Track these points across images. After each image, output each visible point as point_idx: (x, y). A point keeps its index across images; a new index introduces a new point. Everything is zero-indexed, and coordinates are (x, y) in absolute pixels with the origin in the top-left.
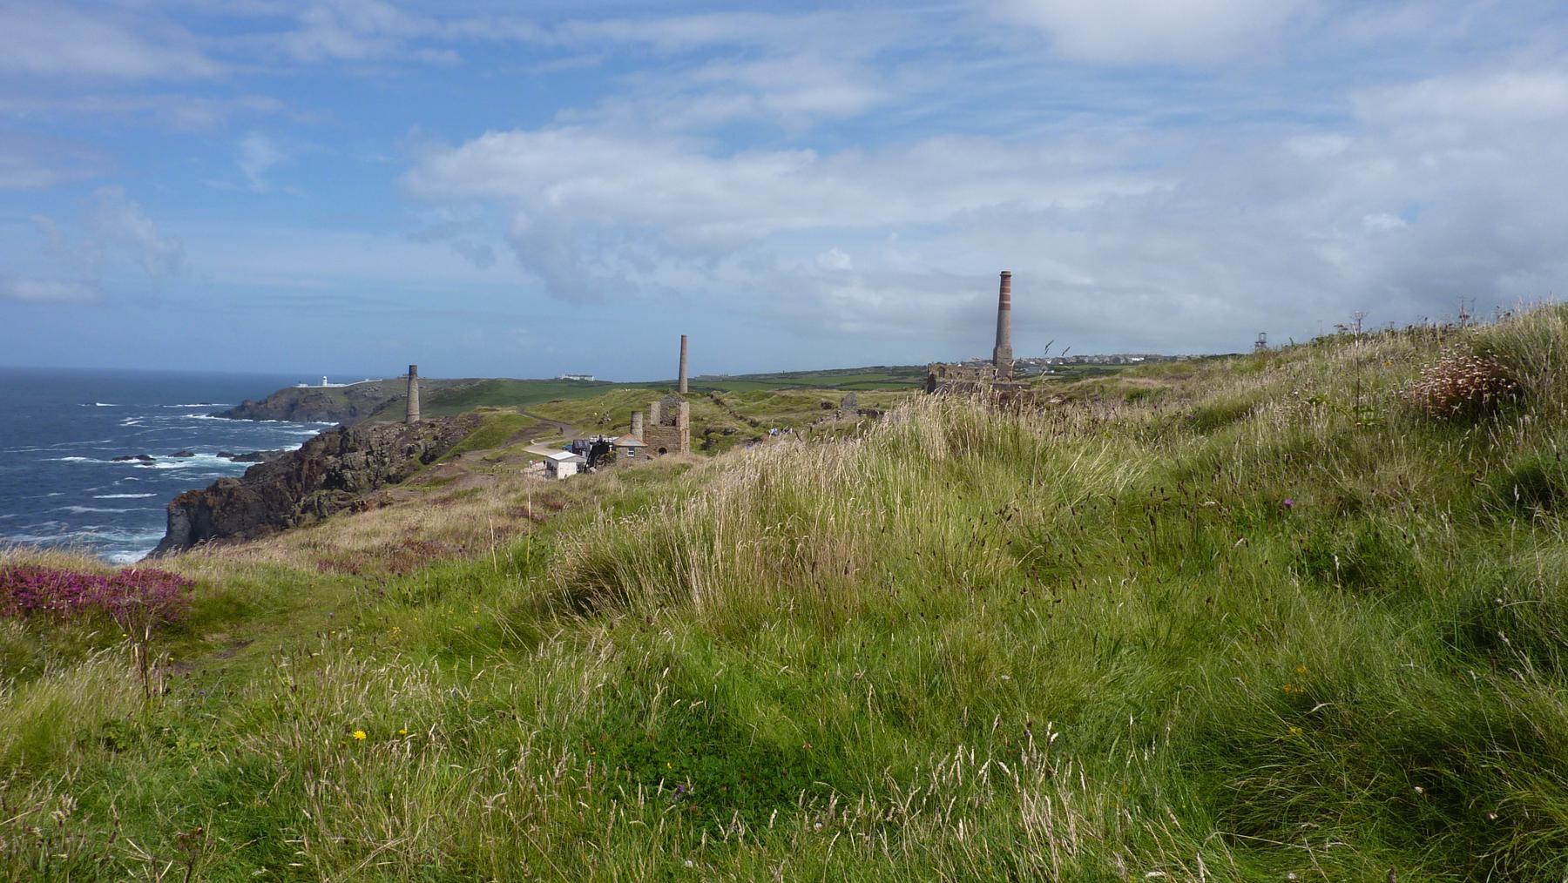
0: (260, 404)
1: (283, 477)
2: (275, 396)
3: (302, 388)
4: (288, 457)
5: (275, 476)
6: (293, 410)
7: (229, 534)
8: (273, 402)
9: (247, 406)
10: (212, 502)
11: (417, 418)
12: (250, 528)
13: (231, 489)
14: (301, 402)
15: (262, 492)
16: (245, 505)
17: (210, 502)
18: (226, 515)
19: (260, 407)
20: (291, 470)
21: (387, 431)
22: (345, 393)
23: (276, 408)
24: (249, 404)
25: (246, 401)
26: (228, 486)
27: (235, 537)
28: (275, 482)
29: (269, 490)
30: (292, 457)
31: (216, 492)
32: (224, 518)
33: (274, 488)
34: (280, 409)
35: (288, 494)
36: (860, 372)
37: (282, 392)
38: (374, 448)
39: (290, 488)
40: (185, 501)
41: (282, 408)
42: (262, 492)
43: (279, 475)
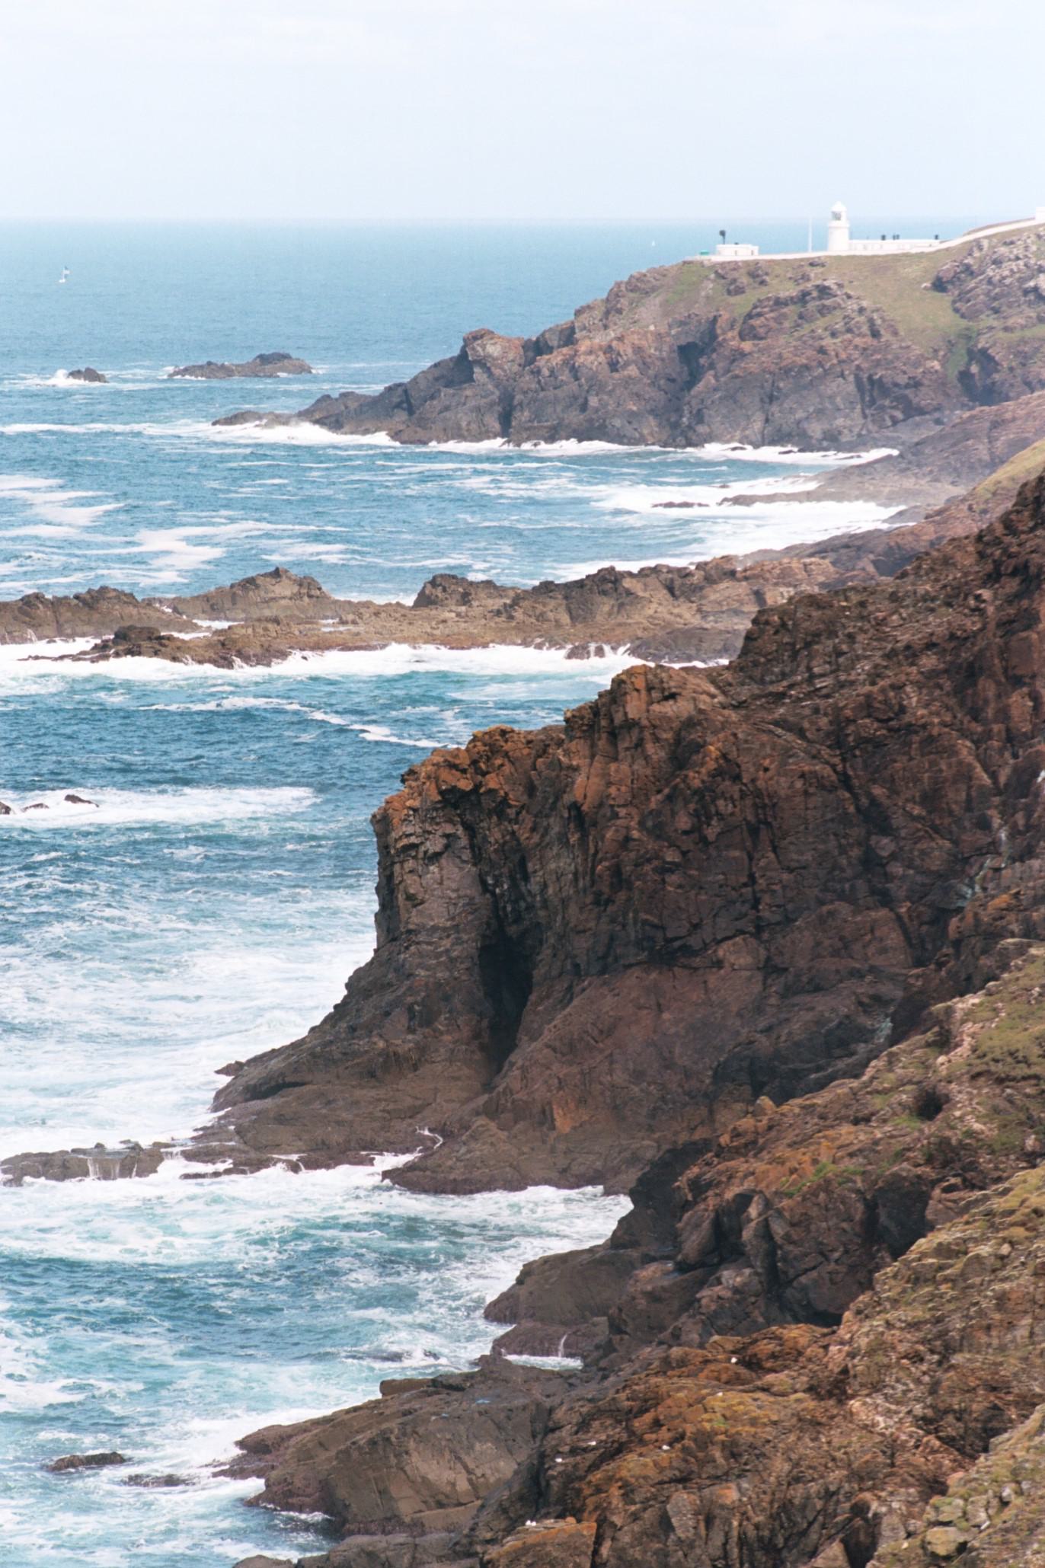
0: (538, 347)
1: (929, 661)
2: (611, 307)
3: (735, 266)
4: (947, 561)
5: (890, 655)
6: (694, 378)
7: (687, 951)
8: (600, 339)
9: (481, 362)
10: (596, 783)
11: (552, 820)
12: (789, 920)
13: (690, 723)
14: (731, 339)
15: (837, 739)
16: (765, 804)
17: (585, 786)
18: (672, 856)
19: (542, 361)
20: (973, 624)
21: (332, 931)
22: (939, 285)
23: (614, 366)
24: (493, 350)
25: (476, 337)
26: (669, 708)
27: (719, 964)
28: (898, 688)
29: (869, 726)
30: (967, 560)
31: (613, 735)
32: (666, 869)
33: (892, 717)
34: (633, 371)
35: (965, 749)
36: (299, 452)
37: (639, 287)
38: (563, 957)
39: (975, 715)
40: (465, 785)
41: (644, 365)
42: (837, 739)
43: (911, 653)
